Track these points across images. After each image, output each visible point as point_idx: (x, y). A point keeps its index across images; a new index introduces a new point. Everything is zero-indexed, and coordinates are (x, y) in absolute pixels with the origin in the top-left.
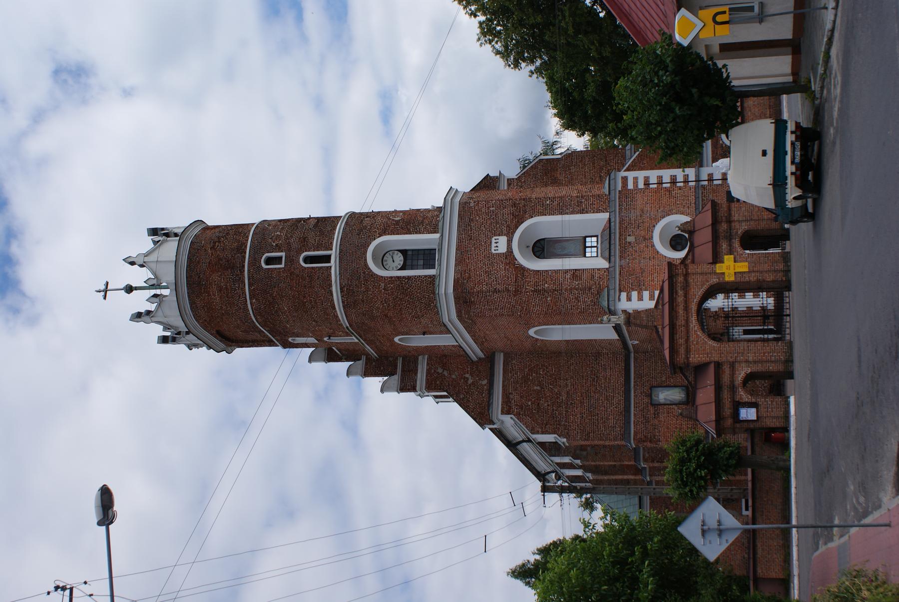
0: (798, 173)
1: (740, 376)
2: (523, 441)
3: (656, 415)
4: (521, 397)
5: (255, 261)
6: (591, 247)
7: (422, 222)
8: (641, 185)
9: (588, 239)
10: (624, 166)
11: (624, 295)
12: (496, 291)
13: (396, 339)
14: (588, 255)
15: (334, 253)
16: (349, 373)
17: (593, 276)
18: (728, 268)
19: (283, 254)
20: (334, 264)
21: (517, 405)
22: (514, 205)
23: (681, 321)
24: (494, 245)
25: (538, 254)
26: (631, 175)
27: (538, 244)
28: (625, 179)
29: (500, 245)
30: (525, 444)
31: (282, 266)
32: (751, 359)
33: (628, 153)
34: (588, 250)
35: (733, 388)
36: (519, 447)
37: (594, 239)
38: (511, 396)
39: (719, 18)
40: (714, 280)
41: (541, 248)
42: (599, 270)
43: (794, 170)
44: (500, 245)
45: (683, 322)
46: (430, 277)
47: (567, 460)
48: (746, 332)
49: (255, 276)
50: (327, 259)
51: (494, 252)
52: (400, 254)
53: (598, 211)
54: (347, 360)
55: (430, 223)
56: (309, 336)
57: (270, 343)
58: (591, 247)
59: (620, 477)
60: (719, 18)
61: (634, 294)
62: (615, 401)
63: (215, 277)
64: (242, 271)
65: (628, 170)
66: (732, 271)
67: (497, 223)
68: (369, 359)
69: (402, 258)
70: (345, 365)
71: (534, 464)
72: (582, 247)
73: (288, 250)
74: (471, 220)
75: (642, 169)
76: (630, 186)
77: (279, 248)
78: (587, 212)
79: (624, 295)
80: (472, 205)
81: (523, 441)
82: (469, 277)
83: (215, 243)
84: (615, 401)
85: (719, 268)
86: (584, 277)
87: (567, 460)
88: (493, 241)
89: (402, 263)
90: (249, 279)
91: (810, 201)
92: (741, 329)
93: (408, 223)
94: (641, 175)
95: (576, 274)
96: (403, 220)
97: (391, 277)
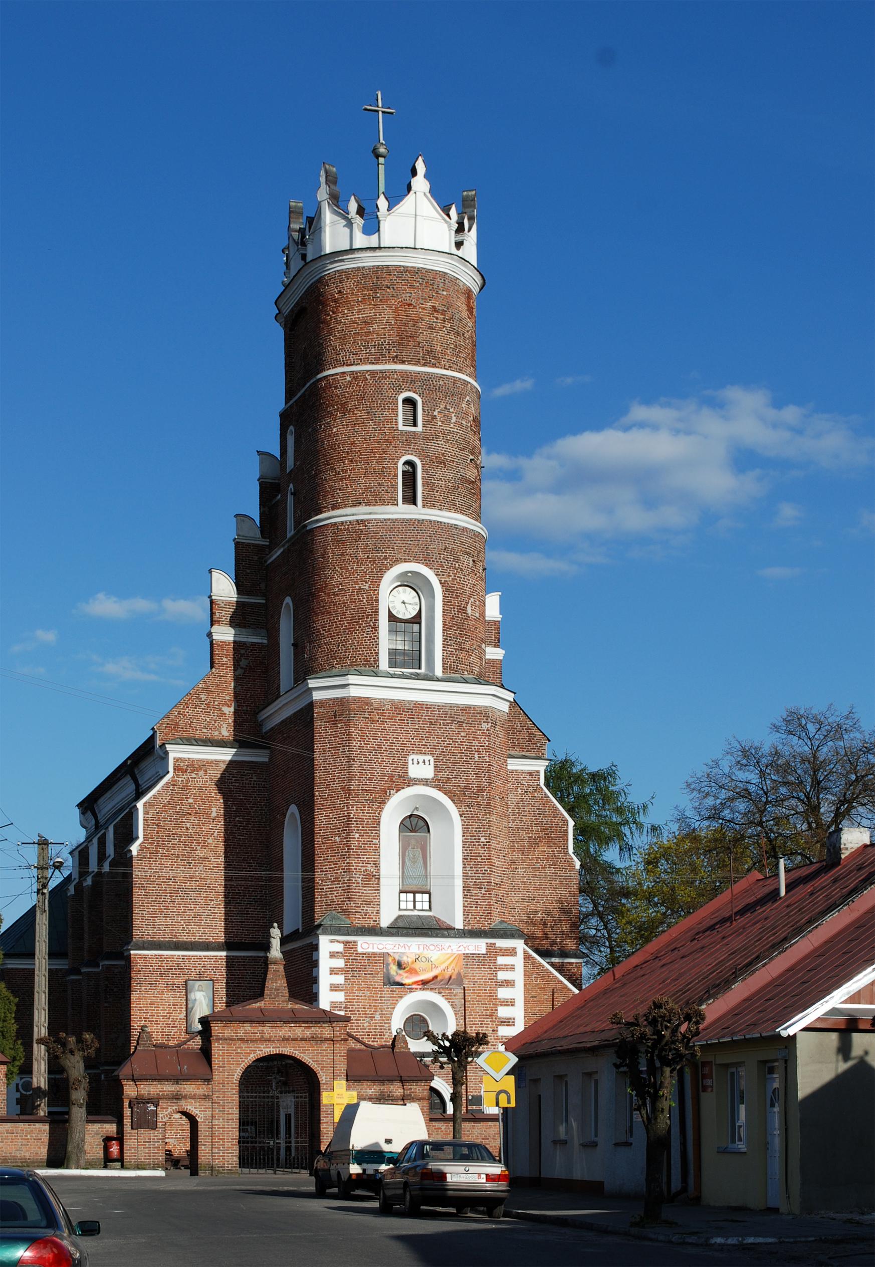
0: (365, 1177)
1: (192, 1107)
2: (138, 785)
3: (172, 987)
4: (200, 789)
5: (410, 380)
6: (414, 901)
7: (462, 649)
8: (502, 976)
9: (426, 896)
10: (537, 951)
11: (340, 948)
12: (350, 760)
13: (288, 600)
14: (403, 896)
15: (418, 512)
16: (241, 518)
17: (368, 903)
18: (340, 1096)
19: (419, 428)
20: (402, 511)
21: (188, 781)
22: (481, 790)
23: (267, 1030)
24: (421, 758)
25: (407, 823)
26: (518, 961)
27: (421, 823)
28: (512, 952)
29: (421, 767)
30: (133, 787)
31: (401, 427)
32: (216, 1122)
33: (553, 960)
34: (410, 896)
35: (177, 1097)
36: (128, 778)
37: (426, 906)
38: (201, 773)
39: (503, 1097)
40: (323, 1077)
41: (414, 825)
42: (378, 912)
43: (367, 1172)
44: (421, 767)
45: (267, 1036)
46: (376, 660)
47: (110, 850)
48: (288, 1117)
49: (387, 381)
50: (411, 499)
51: (410, 758)
52: (414, 613)
53: (466, 913)
54: (262, 515)
55: (458, 660)
56: (296, 460)
57: (289, 393)
58: (414, 901)
59: (86, 929)
60: (503, 1097)
61: (340, 963)
62: (193, 928)
63: (387, 314)
64: (397, 360)
65: (527, 957)
66: (335, 1101)
67: (454, 763)
68: (263, 551)
69: (408, 616)
70: (255, 513)
71: (108, 795)
72: (415, 889)
73: (426, 438)
74: (460, 724)
75: (527, 975)
76: (501, 960)
77: (430, 420)
78: (465, 896)
79: (340, 948)
80: (485, 726)
81: (138, 785)
82: (373, 721)
83: (443, 313)
84: (193, 928)
85: (340, 1085)
86: (368, 891)
87: (110, 850)
88: (427, 758)
89: (400, 616)
90: (381, 372)
91: (335, 1190)
92: (292, 1111)
93: (460, 627)
94: (518, 976)
95: (373, 878)
96: (467, 618)
97: (377, 601)
